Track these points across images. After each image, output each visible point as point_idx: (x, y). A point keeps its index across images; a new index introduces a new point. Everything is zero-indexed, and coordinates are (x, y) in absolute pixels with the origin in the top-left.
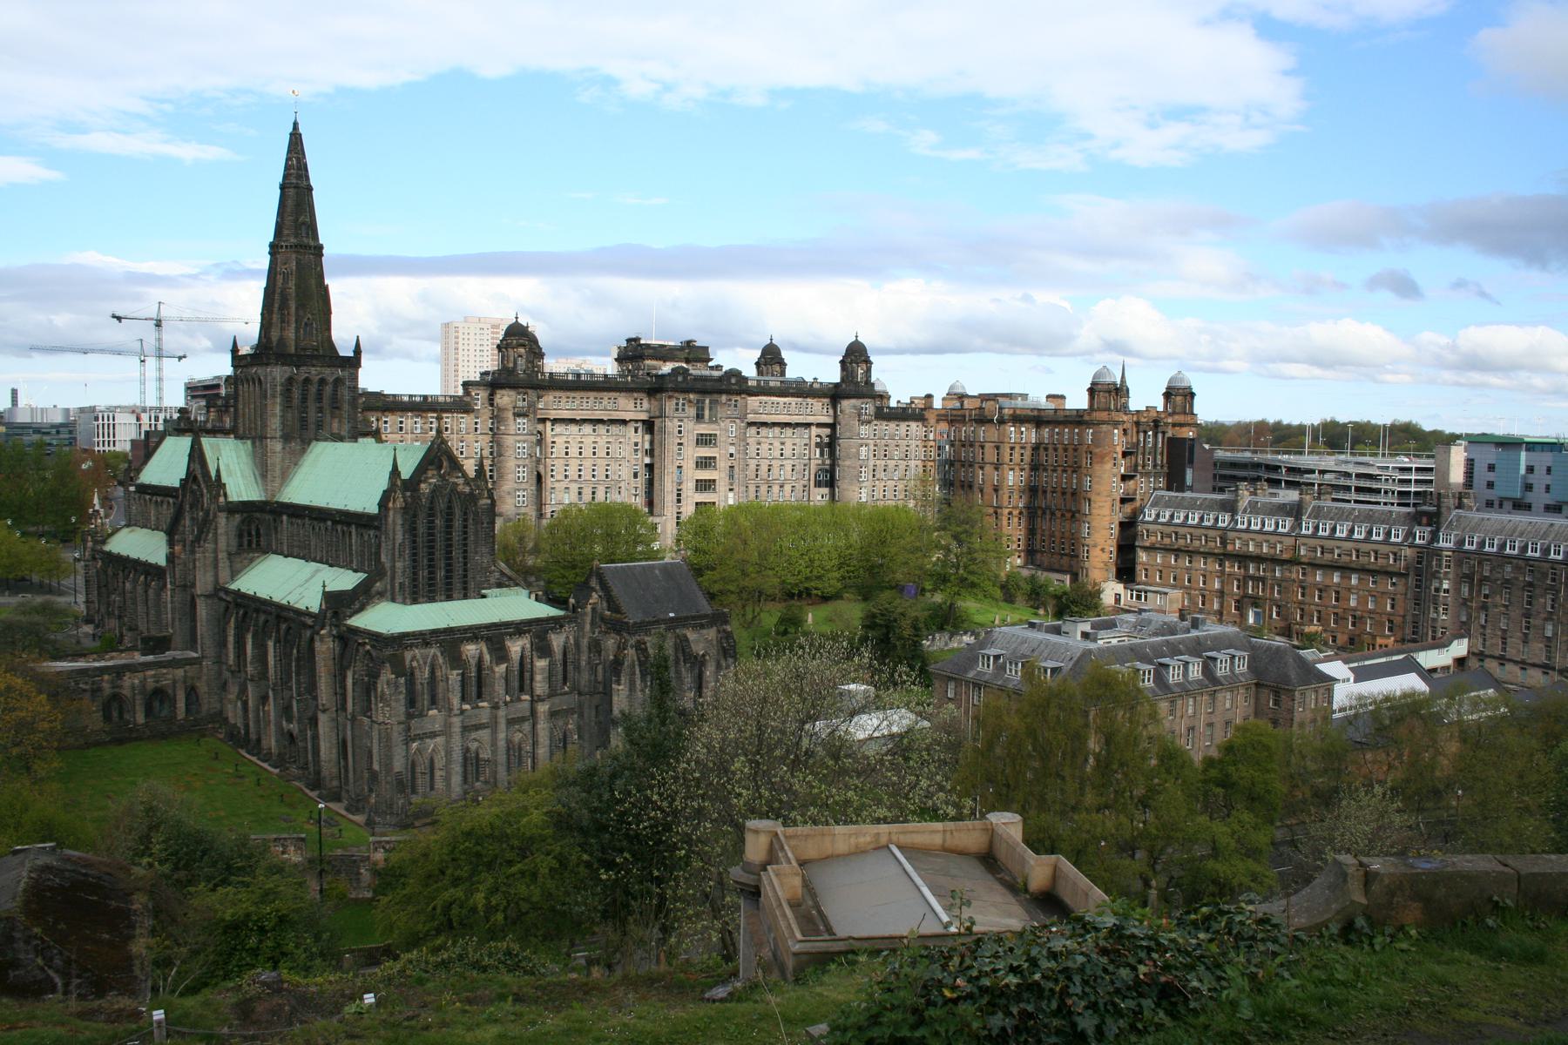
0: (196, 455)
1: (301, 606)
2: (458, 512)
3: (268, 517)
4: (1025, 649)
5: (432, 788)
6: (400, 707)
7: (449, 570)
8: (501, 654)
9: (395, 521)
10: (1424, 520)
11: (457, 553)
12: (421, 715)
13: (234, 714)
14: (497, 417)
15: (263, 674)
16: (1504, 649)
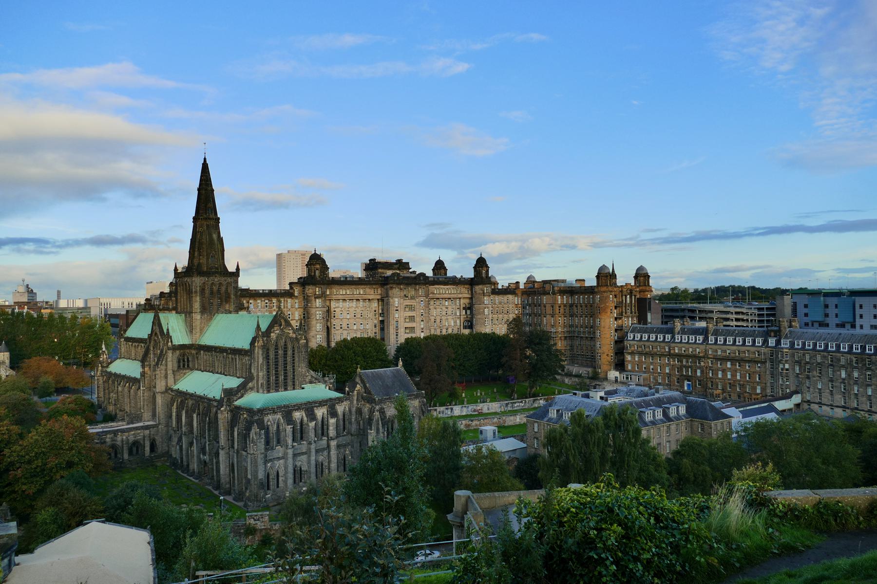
0: (157, 322)
1: (211, 396)
2: (290, 347)
3: (194, 352)
4: (572, 406)
5: (278, 487)
6: (261, 445)
7: (286, 376)
8: (312, 416)
9: (259, 353)
10: (772, 334)
11: (289, 367)
12: (272, 449)
13: (175, 453)
14: (306, 299)
15: (191, 431)
16: (833, 401)
